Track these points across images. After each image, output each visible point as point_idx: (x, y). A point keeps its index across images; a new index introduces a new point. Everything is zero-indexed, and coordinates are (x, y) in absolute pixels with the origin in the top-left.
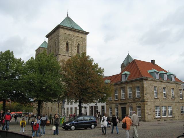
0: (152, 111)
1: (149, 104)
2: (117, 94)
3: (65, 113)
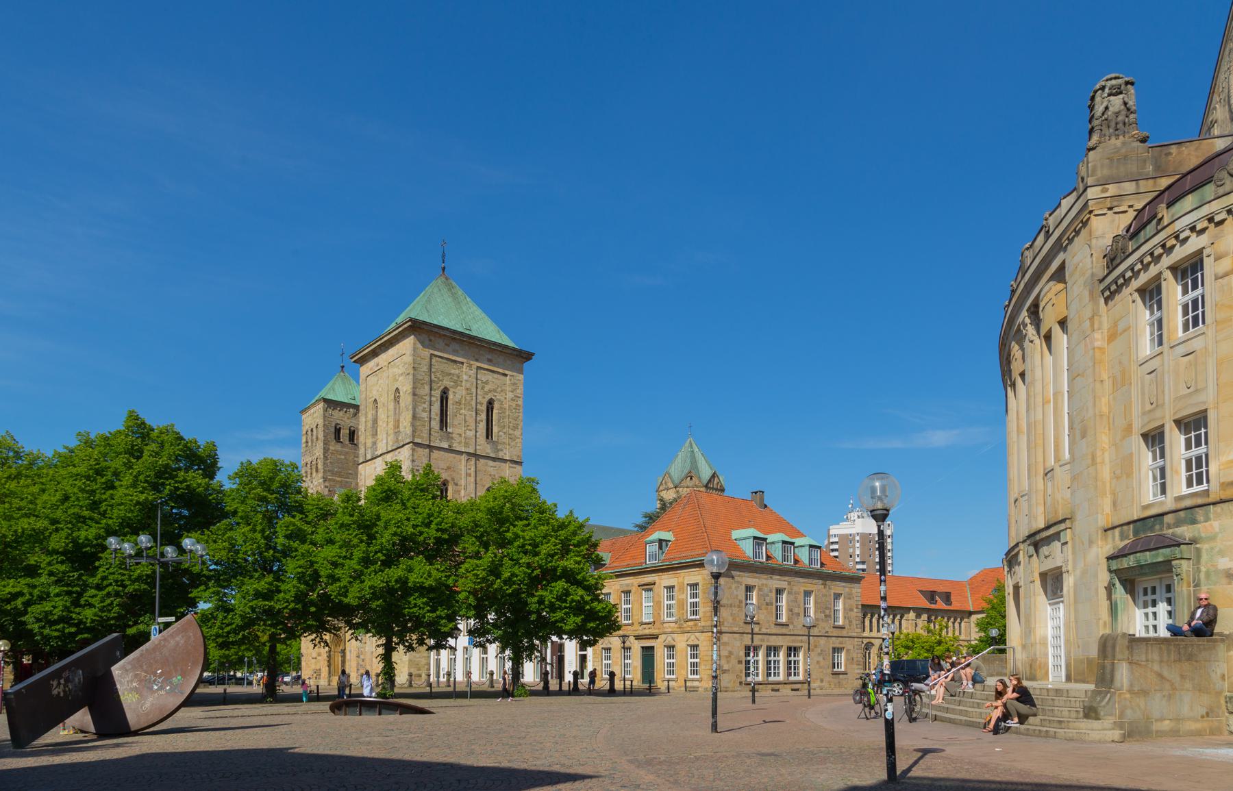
0: (734, 661)
2: (630, 606)
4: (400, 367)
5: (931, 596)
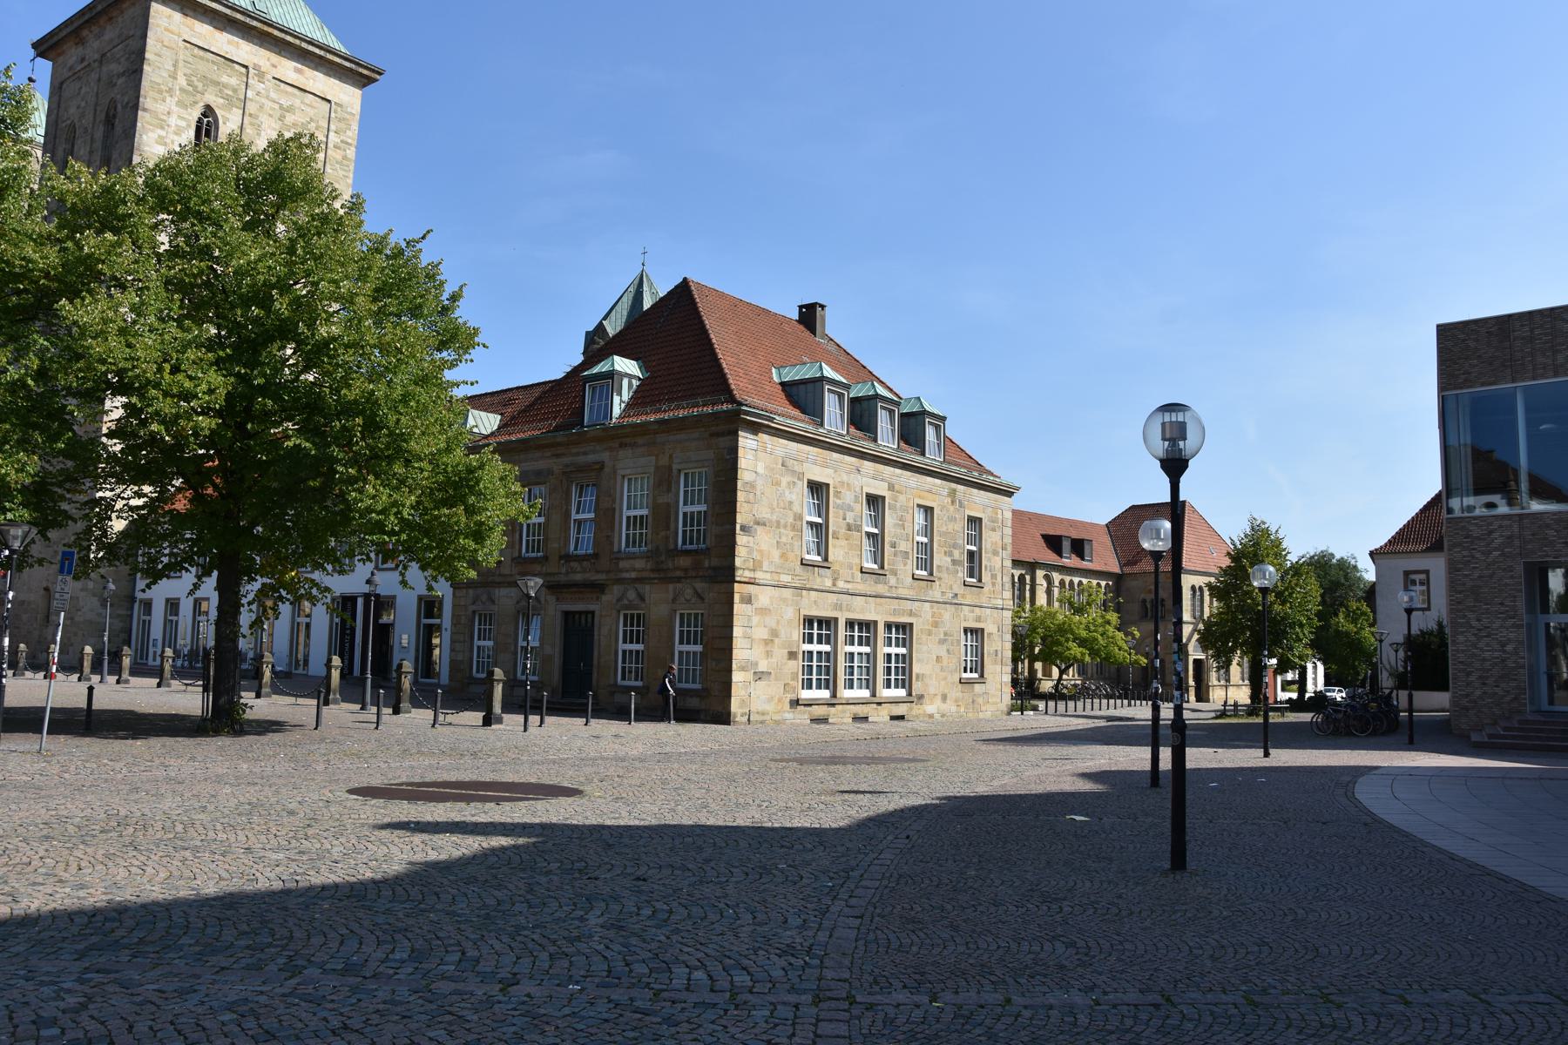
0: (780, 653)
1: (764, 597)
3: (152, 637)
4: (123, 60)
5: (1054, 543)
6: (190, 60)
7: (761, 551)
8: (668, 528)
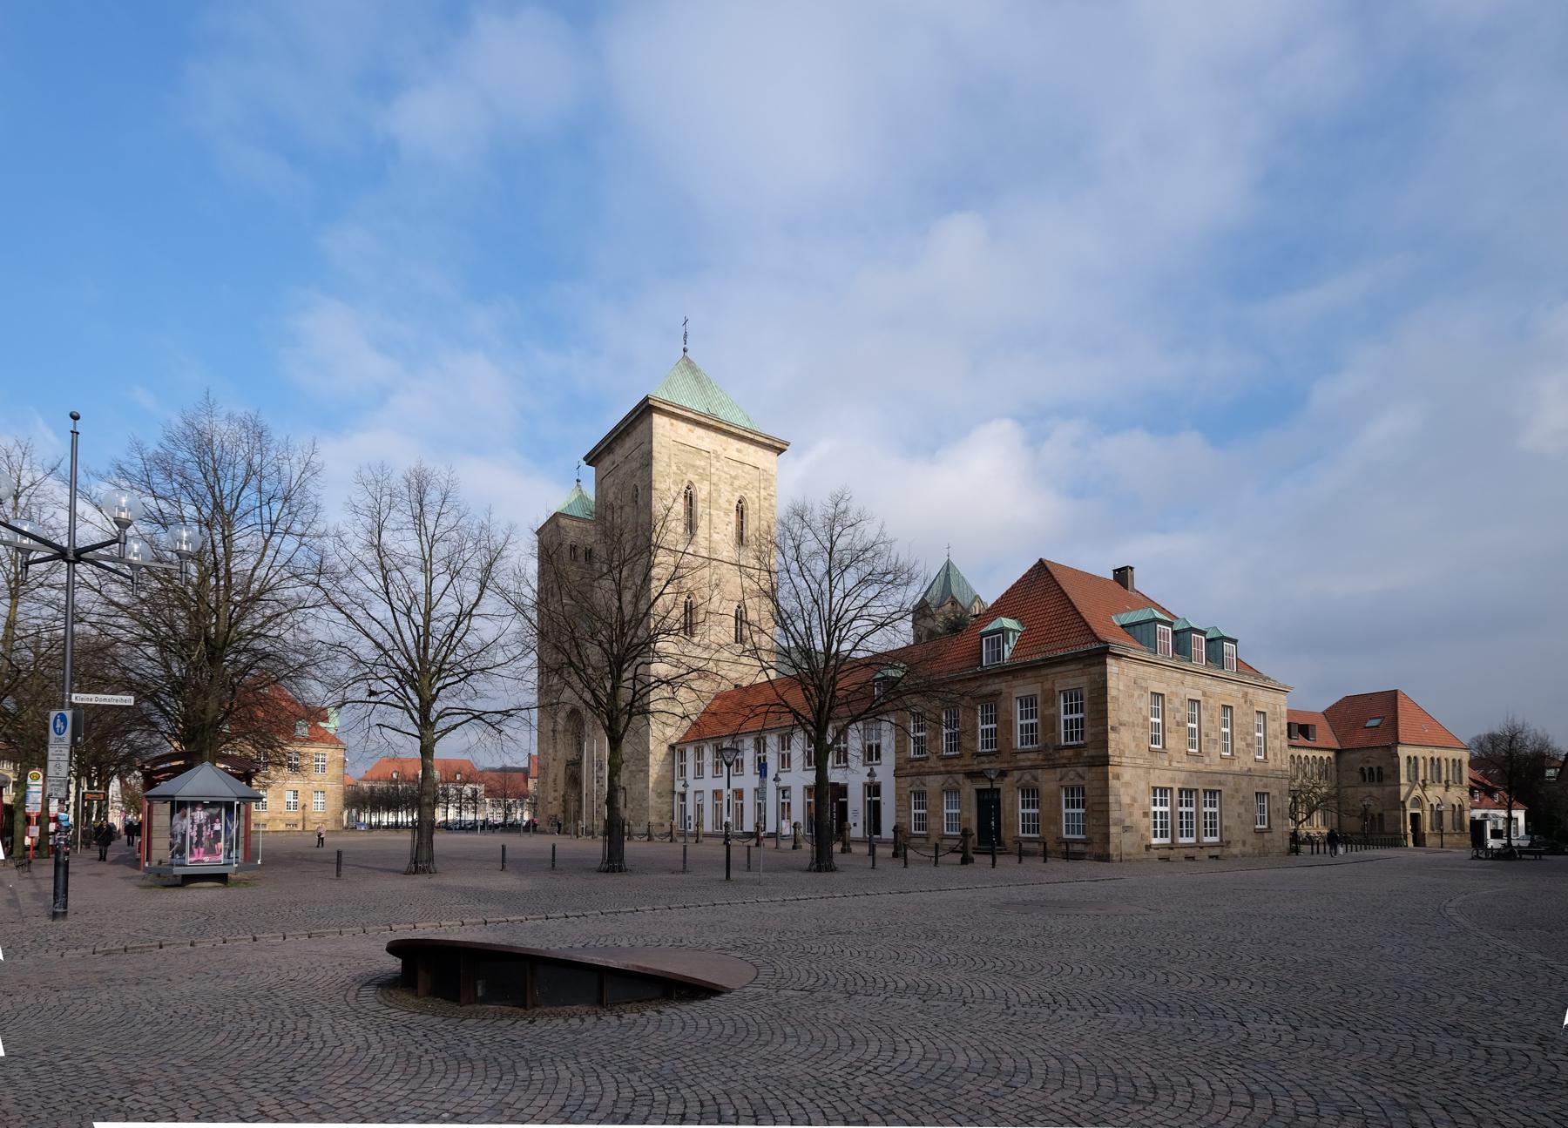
3: (688, 814)
6: (677, 453)
7: (1124, 743)
8: (1053, 731)
